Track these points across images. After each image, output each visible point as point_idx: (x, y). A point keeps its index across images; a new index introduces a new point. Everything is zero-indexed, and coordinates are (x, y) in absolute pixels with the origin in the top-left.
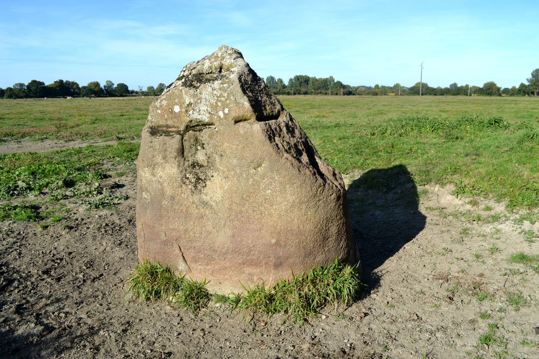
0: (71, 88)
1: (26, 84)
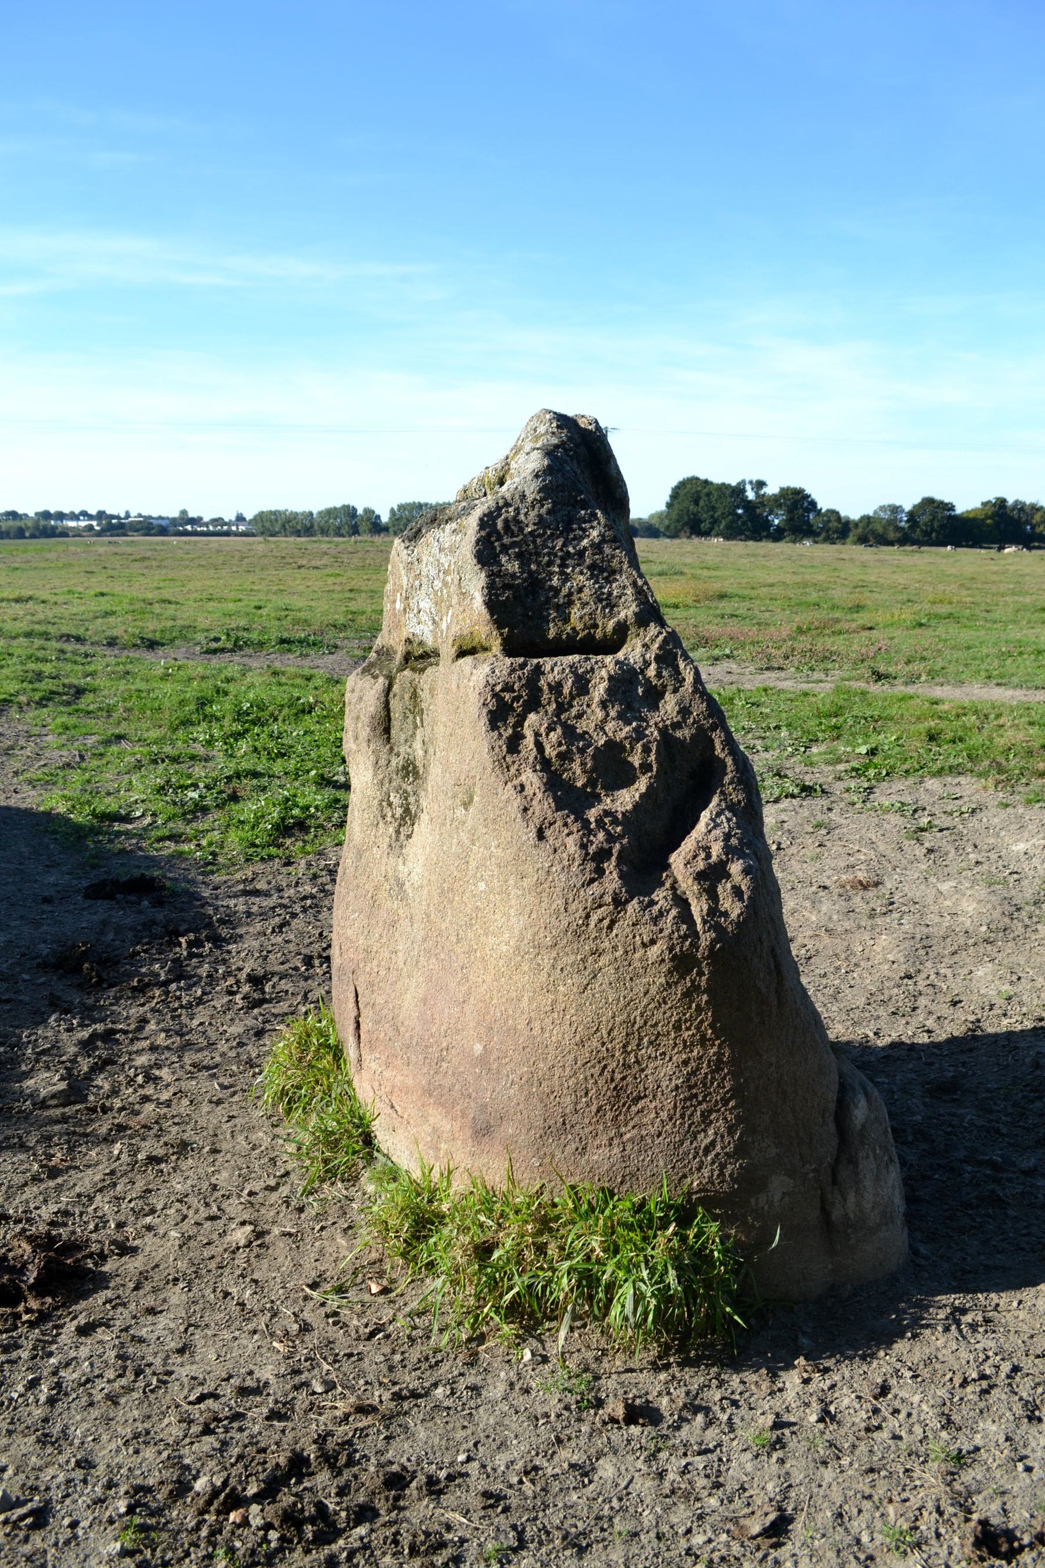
0: (1027, 522)
1: (908, 507)
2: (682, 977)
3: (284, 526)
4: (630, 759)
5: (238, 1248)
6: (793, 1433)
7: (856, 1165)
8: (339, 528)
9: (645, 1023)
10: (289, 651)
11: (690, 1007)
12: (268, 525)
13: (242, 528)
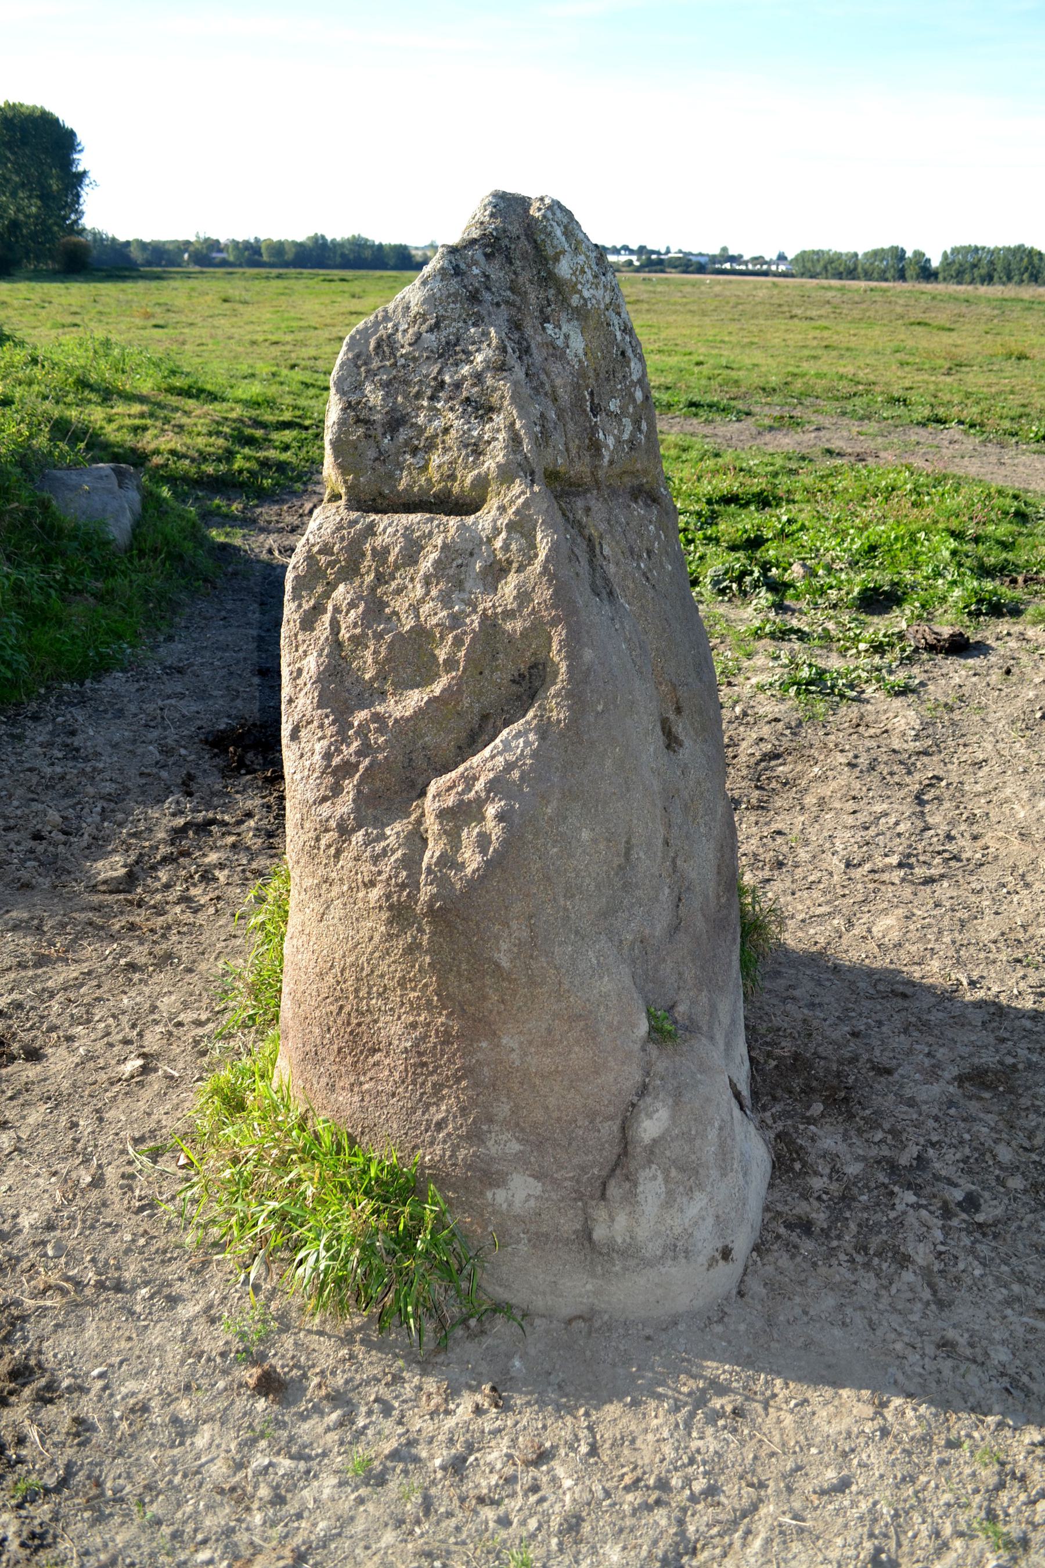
2: (403, 931)
3: (825, 268)
4: (436, 652)
5: (120, 1080)
6: (405, 1472)
7: (636, 1185)
8: (885, 272)
9: (372, 972)
10: (696, 415)
11: (413, 966)
12: (809, 265)
13: (782, 268)
